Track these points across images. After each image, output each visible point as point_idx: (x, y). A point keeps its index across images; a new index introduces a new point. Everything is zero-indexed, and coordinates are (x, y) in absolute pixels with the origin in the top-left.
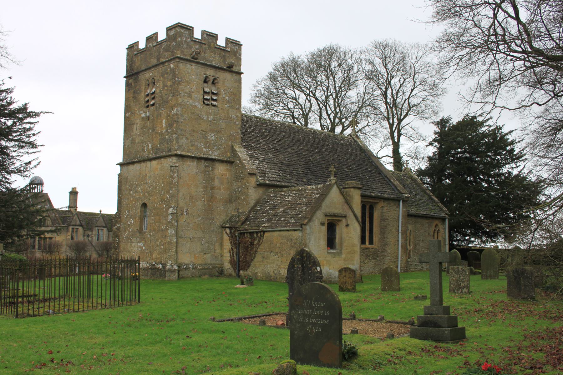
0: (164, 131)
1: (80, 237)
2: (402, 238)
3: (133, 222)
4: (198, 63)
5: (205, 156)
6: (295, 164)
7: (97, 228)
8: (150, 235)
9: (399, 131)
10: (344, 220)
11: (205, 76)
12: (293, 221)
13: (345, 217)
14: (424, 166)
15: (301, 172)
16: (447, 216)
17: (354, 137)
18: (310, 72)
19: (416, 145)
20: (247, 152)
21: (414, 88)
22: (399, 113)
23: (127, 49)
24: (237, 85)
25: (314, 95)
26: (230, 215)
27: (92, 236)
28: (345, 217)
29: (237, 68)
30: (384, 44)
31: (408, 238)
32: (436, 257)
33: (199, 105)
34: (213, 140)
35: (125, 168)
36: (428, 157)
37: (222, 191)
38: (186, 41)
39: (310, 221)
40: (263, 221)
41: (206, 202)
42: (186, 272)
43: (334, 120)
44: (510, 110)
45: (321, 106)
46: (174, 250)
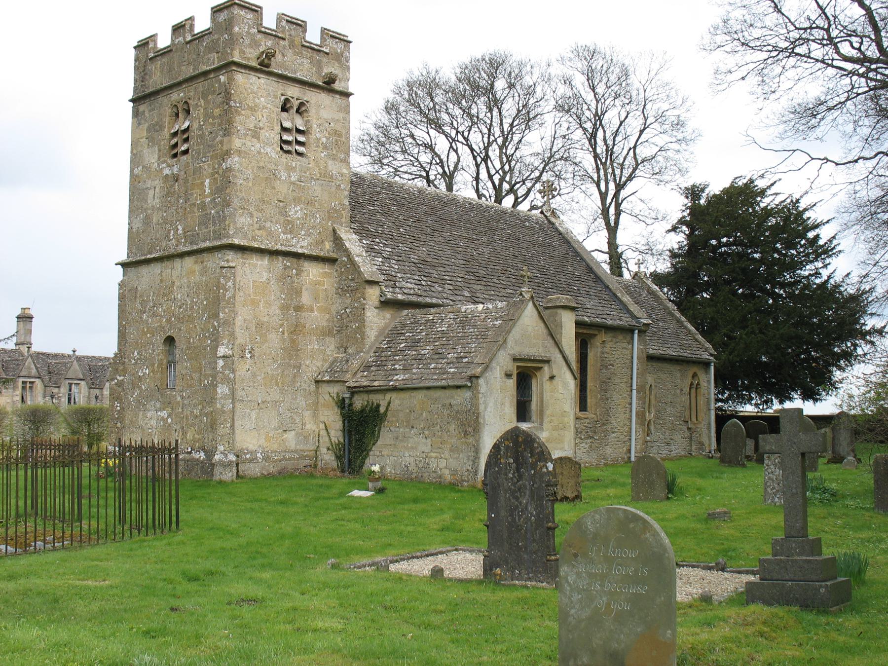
0: (208, 200)
1: (38, 399)
2: (638, 398)
3: (147, 371)
4: (271, 74)
5: (284, 248)
6: (447, 263)
7: (68, 382)
8: (182, 398)
9: (618, 206)
10: (546, 368)
11: (283, 98)
12: (452, 370)
13: (548, 362)
14: (664, 266)
15: (460, 280)
16: (712, 358)
17: (548, 214)
18: (457, 97)
19: (650, 228)
20: (360, 241)
21: (645, 129)
22: (618, 172)
23: (135, 48)
24: (341, 115)
25: (467, 139)
26: (331, 359)
27: (59, 397)
28: (548, 362)
29: (343, 84)
30: (591, 49)
31: (647, 400)
32: (795, 443)
33: (273, 151)
34: (298, 219)
35: (132, 271)
36: (670, 251)
37: (316, 313)
38: (248, 33)
39: (486, 369)
40: (395, 369)
41: (286, 334)
42: (251, 465)
43: (501, 184)
44: (837, 164)
45: (479, 159)
46: (229, 425)
